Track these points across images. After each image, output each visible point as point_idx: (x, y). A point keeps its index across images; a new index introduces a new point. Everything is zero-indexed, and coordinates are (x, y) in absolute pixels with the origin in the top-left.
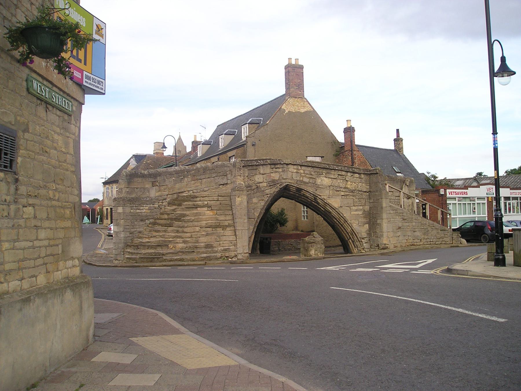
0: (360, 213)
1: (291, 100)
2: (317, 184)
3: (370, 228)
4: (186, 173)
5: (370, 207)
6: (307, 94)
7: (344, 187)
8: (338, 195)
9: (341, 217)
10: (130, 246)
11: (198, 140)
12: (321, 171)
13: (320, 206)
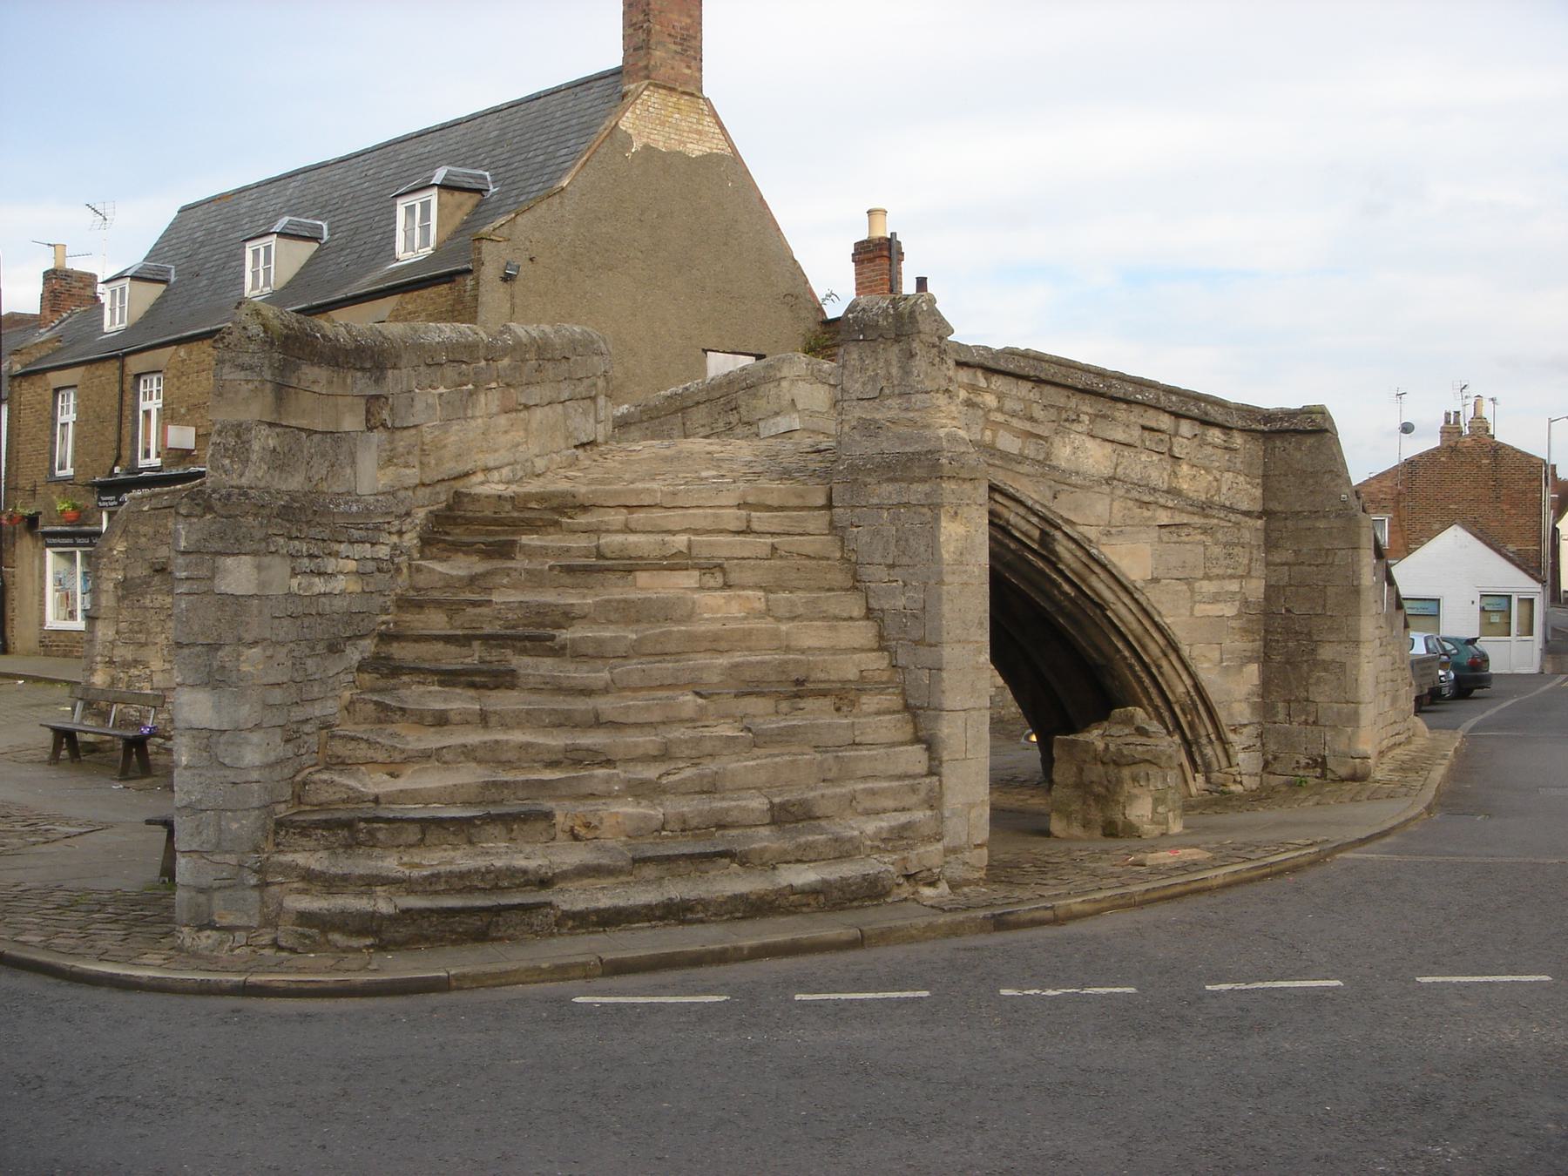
0: (1229, 610)
1: (652, 99)
2: (1054, 467)
3: (1266, 684)
4: (483, 363)
5: (1268, 587)
6: (716, 80)
7: (1165, 487)
8: (1145, 524)
9: (1152, 630)
10: (305, 830)
12: (1073, 403)
13: (1061, 573)
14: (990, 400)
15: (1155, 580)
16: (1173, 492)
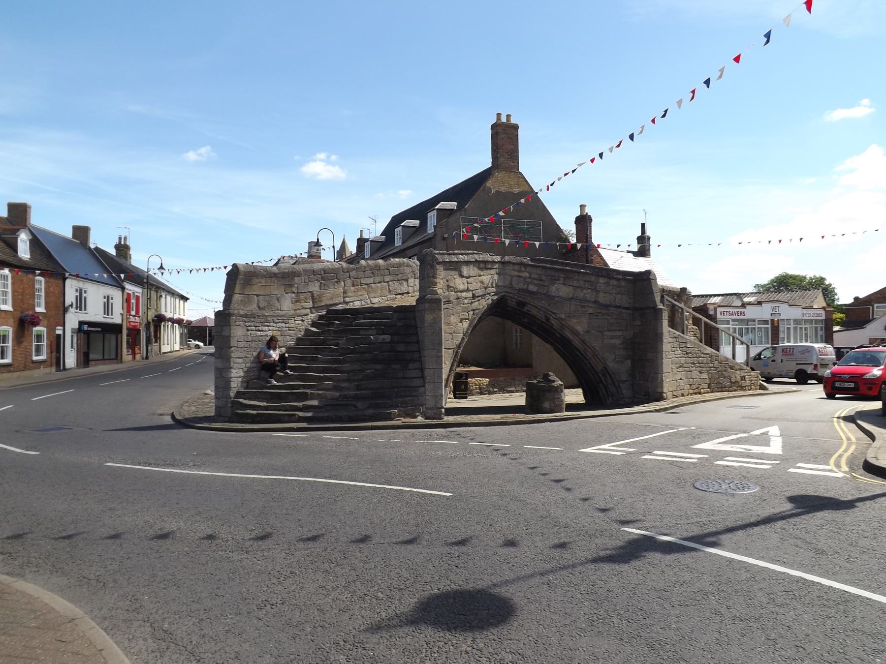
0: (617, 342)
7: (593, 300)
11: (365, 236)
14: (528, 275)
15: (588, 332)
16: (595, 302)
